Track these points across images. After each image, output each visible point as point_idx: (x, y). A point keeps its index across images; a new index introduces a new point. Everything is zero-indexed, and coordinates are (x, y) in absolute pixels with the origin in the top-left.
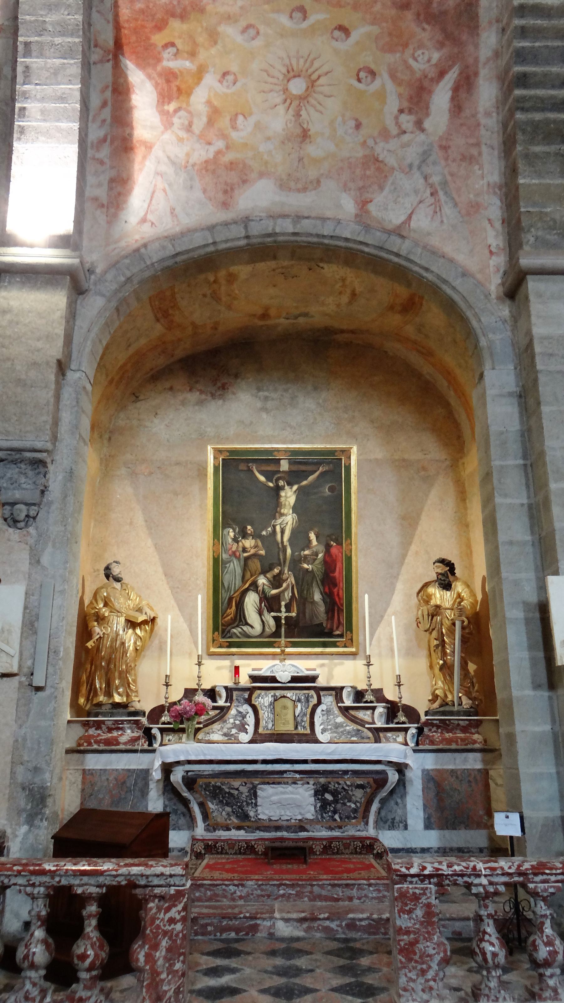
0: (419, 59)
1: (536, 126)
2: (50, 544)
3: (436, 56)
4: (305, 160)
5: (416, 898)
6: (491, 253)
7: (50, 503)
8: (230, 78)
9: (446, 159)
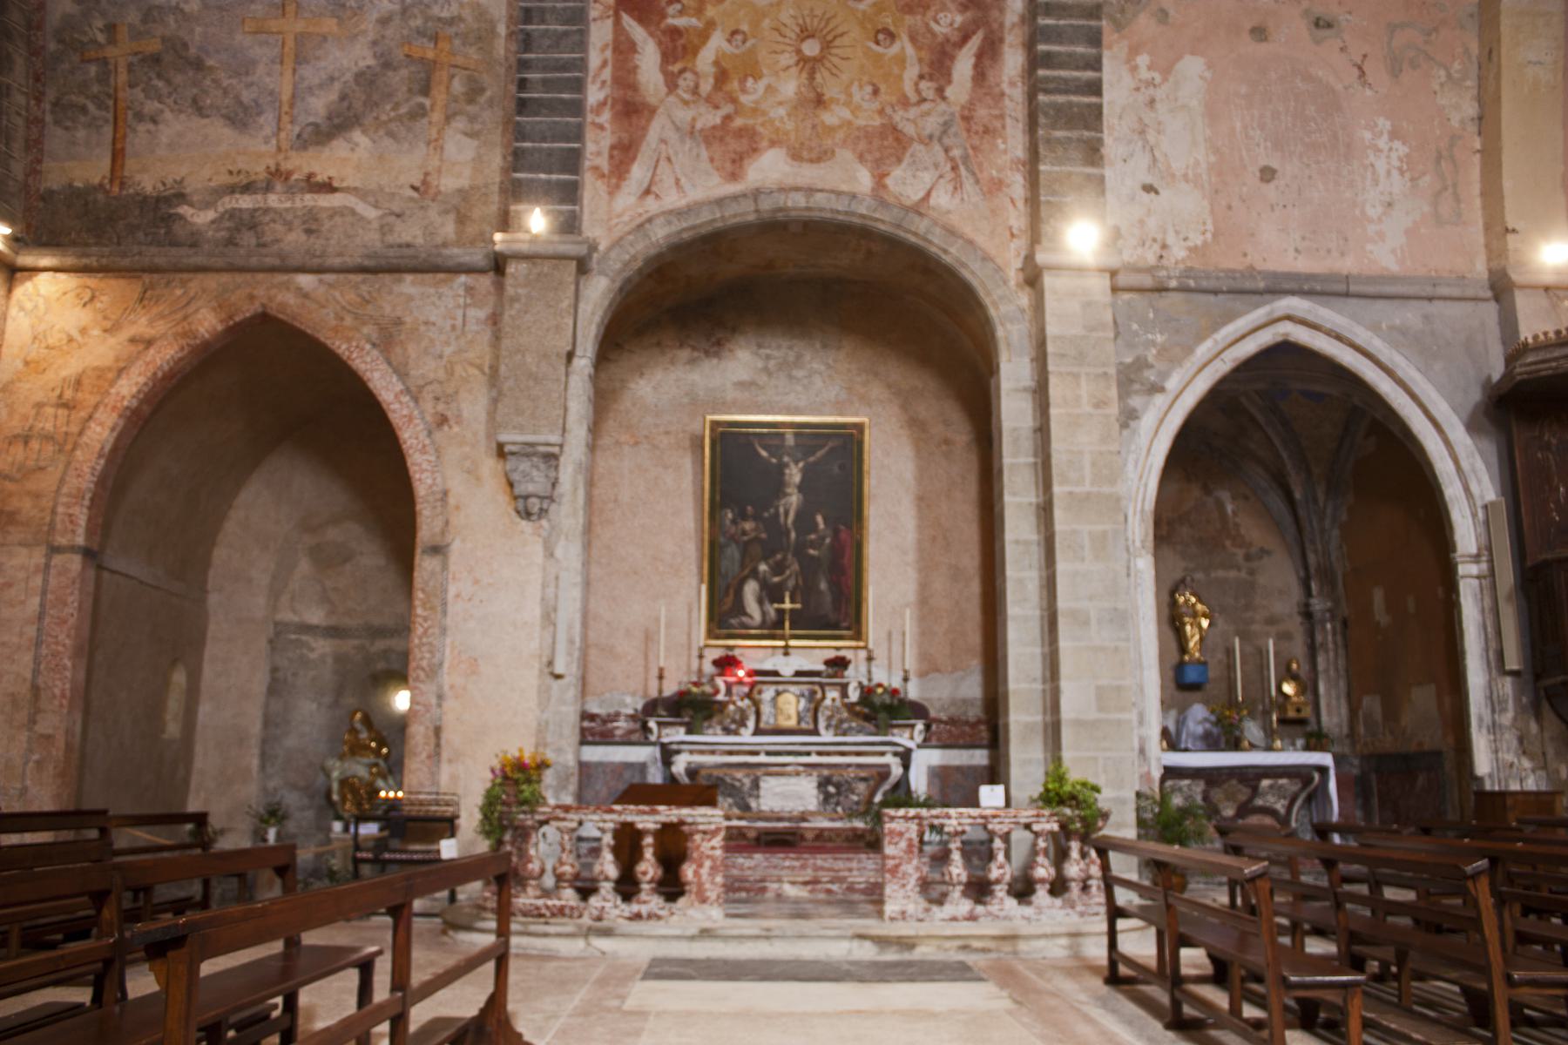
0: (942, 22)
1: (1058, 109)
2: (563, 537)
3: (959, 19)
4: (820, 129)
5: (901, 834)
6: (1013, 235)
7: (561, 496)
8: (739, 37)
9: (968, 131)
